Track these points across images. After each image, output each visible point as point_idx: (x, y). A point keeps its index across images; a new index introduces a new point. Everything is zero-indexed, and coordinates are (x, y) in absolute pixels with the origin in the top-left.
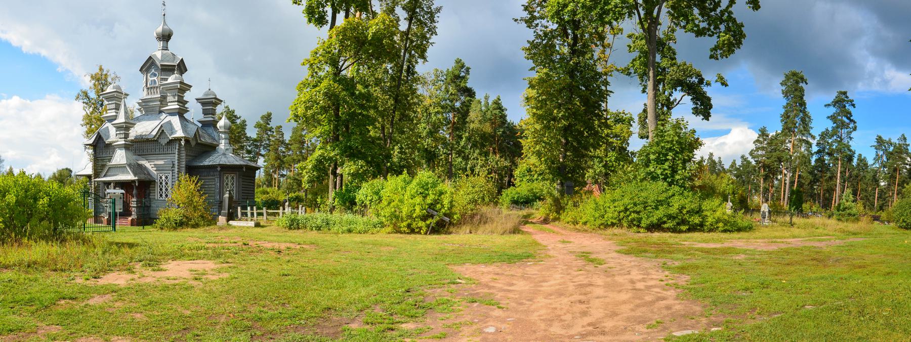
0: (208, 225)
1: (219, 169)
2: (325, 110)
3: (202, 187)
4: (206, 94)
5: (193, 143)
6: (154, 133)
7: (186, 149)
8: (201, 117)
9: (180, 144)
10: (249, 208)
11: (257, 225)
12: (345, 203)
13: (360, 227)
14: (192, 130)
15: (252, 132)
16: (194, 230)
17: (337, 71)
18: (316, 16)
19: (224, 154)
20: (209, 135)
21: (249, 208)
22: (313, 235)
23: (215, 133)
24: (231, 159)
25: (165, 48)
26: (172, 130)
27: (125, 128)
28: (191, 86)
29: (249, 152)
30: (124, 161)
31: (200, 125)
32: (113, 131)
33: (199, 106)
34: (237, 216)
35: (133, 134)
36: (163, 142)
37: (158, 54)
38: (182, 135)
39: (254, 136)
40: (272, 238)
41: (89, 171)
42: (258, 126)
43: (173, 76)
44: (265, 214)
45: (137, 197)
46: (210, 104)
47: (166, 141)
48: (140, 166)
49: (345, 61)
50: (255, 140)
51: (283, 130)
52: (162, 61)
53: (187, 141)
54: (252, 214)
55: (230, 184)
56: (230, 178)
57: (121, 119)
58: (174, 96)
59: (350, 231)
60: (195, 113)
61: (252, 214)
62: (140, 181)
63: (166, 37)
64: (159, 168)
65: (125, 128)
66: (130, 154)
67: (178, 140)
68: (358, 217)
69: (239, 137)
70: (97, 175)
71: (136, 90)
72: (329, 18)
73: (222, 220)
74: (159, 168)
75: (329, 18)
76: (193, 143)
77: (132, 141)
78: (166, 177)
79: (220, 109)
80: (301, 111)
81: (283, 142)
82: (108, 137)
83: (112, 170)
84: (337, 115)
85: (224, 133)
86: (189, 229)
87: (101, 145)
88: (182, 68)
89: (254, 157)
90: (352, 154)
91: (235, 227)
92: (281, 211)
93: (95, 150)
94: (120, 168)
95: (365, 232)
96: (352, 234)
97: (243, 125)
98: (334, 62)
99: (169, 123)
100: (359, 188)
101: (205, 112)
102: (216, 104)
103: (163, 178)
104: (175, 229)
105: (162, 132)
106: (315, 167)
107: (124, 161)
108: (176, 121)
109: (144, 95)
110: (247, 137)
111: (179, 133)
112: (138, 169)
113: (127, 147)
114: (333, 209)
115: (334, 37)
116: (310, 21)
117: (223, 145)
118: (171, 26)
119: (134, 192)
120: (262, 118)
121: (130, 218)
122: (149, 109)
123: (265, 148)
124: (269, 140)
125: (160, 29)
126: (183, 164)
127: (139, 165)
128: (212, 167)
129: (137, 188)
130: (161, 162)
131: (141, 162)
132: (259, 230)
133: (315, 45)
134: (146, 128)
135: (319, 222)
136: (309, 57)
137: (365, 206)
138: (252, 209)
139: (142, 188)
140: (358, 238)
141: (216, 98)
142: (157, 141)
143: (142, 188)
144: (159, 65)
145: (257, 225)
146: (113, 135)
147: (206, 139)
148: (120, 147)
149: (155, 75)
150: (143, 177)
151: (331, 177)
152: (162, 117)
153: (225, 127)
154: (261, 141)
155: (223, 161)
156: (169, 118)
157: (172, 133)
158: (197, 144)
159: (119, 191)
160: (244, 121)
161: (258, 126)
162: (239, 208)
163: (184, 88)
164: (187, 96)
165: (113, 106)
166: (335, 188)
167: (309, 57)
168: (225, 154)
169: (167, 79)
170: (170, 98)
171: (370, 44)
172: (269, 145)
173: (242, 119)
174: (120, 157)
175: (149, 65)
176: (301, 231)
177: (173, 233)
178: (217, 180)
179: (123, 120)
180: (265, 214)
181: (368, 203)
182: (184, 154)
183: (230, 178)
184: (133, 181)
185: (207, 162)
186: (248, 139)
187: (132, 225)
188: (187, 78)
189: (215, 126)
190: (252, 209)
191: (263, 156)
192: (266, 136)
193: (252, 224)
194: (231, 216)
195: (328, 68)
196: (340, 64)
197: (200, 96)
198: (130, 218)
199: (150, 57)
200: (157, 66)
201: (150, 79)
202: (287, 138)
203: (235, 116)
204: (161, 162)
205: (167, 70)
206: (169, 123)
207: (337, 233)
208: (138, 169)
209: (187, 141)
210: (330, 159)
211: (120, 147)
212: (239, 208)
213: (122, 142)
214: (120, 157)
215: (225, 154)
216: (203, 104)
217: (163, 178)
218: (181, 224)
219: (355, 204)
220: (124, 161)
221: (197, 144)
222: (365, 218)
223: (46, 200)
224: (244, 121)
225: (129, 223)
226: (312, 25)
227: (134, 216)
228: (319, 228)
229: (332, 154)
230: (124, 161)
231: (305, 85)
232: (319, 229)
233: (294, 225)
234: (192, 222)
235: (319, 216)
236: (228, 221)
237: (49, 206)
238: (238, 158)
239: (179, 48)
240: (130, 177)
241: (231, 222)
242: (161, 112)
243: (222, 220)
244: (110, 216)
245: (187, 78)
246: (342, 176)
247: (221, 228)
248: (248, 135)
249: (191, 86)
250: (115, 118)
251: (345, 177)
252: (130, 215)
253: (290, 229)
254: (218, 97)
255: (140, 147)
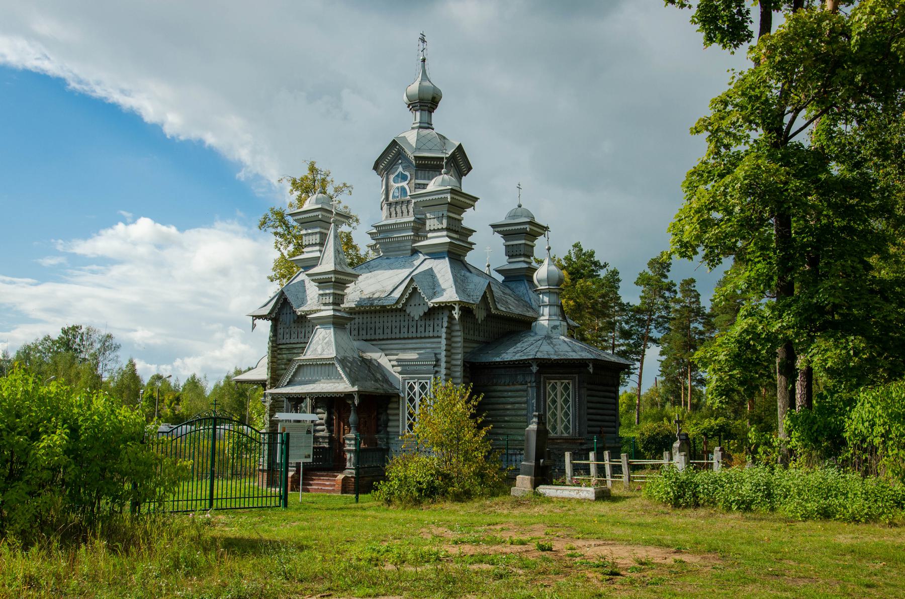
0: (493, 495)
1: (535, 369)
2: (749, 225)
3: (480, 409)
4: (513, 215)
5: (480, 315)
6: (397, 294)
7: (465, 329)
8: (503, 261)
9: (451, 318)
10: (592, 455)
11: (603, 496)
12: (816, 441)
13: (856, 505)
14: (477, 287)
15: (631, 295)
16: (457, 506)
17: (779, 136)
18: (722, 24)
19: (548, 337)
20: (519, 299)
21: (592, 455)
22: (731, 523)
23: (532, 295)
24: (566, 348)
25: (426, 125)
26: (435, 288)
27: (336, 283)
28: (475, 199)
29: (626, 335)
30: (331, 353)
31: (500, 278)
32: (313, 291)
33: (499, 241)
34: (563, 472)
35: (354, 294)
36: (416, 312)
37: (412, 137)
38: (455, 298)
39: (636, 302)
40: (619, 531)
41: (262, 373)
42: (643, 280)
43: (438, 179)
44: (625, 469)
45: (358, 429)
46: (521, 234)
47: (421, 311)
48: (369, 365)
49: (797, 111)
50: (638, 310)
51: (698, 287)
52: (418, 149)
53: (466, 311)
54: (601, 470)
55: (560, 401)
56: (559, 388)
57: (327, 265)
58: (440, 219)
59: (826, 514)
60: (488, 253)
61: (601, 470)
62: (361, 395)
63: (426, 103)
64: (406, 367)
65: (336, 283)
66: (345, 338)
67: (447, 307)
68: (854, 476)
69: (605, 305)
70: (275, 379)
71: (367, 205)
72: (754, 26)
73: (523, 482)
74: (406, 367)
75: (754, 26)
76: (480, 315)
77: (351, 311)
78: (423, 387)
79: (540, 244)
80: (690, 231)
81: (699, 312)
82: (303, 301)
83: (306, 370)
84: (784, 236)
85: (548, 292)
86: (448, 505)
87: (286, 318)
88: (459, 163)
89: (637, 345)
90: (817, 321)
91: (550, 500)
92: (665, 461)
93: (274, 329)
94: (323, 366)
95: (871, 519)
96: (832, 524)
97: (614, 279)
98: (773, 122)
99: (430, 273)
100: (851, 403)
101: (511, 252)
102: (533, 236)
103: (417, 388)
104: (417, 502)
105: (412, 293)
106: (737, 359)
107: (331, 353)
108: (443, 269)
109: (383, 218)
110: (621, 304)
111: (449, 294)
112: (361, 368)
113: (338, 323)
114: (788, 457)
115: (764, 61)
116: (710, 39)
117: (545, 319)
118: (439, 79)
119: (352, 418)
120: (652, 264)
121: (340, 477)
122: (391, 245)
123: (658, 325)
124: (667, 308)
125: (414, 88)
126: (459, 359)
127: (364, 360)
128: (521, 366)
129: (358, 410)
130: (413, 356)
131: (370, 355)
132: (604, 507)
133: (722, 86)
134: (380, 283)
135: (746, 489)
136: (710, 113)
137: (873, 449)
138: (600, 457)
139: (371, 410)
140: (845, 536)
141: (532, 223)
142: (402, 310)
143: (371, 410)
144: (411, 155)
145: (603, 496)
146: (313, 300)
147: (509, 306)
148: (323, 322)
149: (404, 178)
150: (370, 386)
151: (780, 379)
152: (417, 263)
153: (549, 280)
154: (650, 311)
155: (546, 351)
156: (429, 264)
157: (434, 294)
158: (490, 316)
159: (321, 416)
160: (615, 273)
161: (643, 280)
162: (567, 455)
163: (460, 202)
164: (469, 219)
165: (316, 239)
166: (792, 405)
167: (710, 113)
168: (550, 336)
169: (424, 186)
170: (431, 223)
171: (855, 63)
172: (669, 320)
173: (611, 268)
174: (323, 344)
175: (391, 158)
176: (702, 512)
177: (411, 514)
178: (532, 392)
179: (331, 267)
180: (625, 469)
181: (877, 441)
182: (459, 338)
183: (559, 388)
184: (349, 396)
185: (511, 354)
186: (623, 308)
187: (344, 490)
188: (468, 185)
189: (531, 280)
190: (600, 457)
191: (655, 341)
192: (659, 301)
193: (589, 492)
194: (545, 474)
195: (758, 134)
196: (787, 119)
197: (501, 219)
198: (340, 477)
199: (394, 143)
200: (405, 158)
201: (394, 185)
202: (706, 304)
203: (596, 264)
204: (413, 356)
205: (428, 166)
206: (430, 273)
207: (788, 521)
208: (361, 368)
209: (466, 311)
210: (771, 338)
211: (323, 322)
212: (567, 455)
213: (329, 312)
214: (323, 344)
215: (550, 336)
216: (507, 235)
217: (417, 388)
218: (430, 492)
219: (844, 442)
220: (331, 352)
221: (490, 316)
222: (871, 481)
223: (58, 438)
224: (615, 273)
225: (339, 486)
226: (716, 47)
227: (350, 471)
228: (746, 506)
229: (776, 326)
230: (331, 352)
231: (701, 174)
232: (748, 509)
233: (684, 497)
234: (457, 488)
235: (748, 475)
236: (536, 484)
237: (67, 452)
238: (578, 345)
239: (451, 125)
240: (342, 385)
241: (542, 489)
242: (415, 252)
243: (523, 482)
244: (298, 471)
245: (468, 185)
246: (809, 373)
247: (518, 503)
248: (624, 300)
249: (475, 199)
250: (315, 262)
251: (822, 379)
252: (342, 468)
253: (676, 505)
254: (537, 220)
255: (369, 322)
